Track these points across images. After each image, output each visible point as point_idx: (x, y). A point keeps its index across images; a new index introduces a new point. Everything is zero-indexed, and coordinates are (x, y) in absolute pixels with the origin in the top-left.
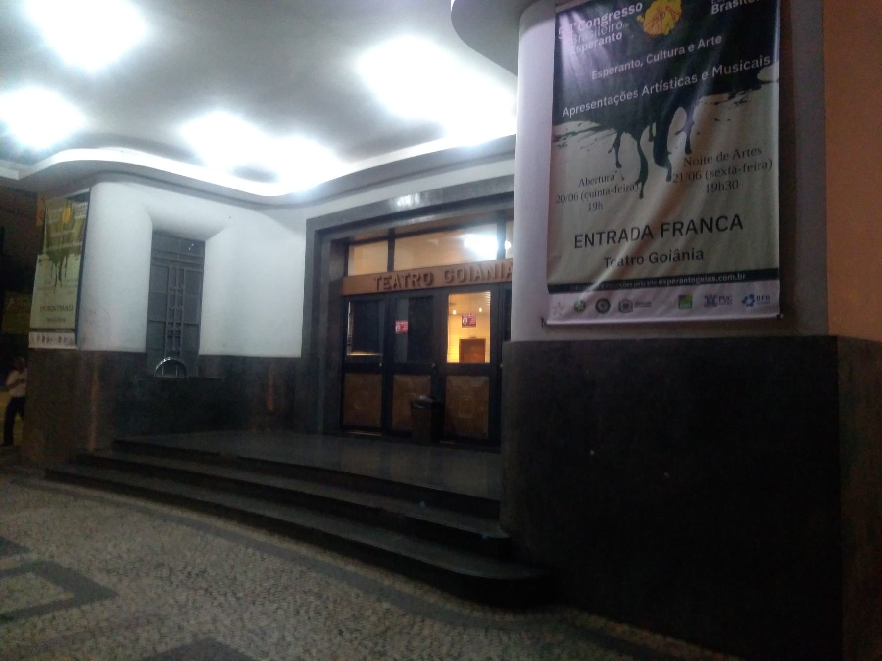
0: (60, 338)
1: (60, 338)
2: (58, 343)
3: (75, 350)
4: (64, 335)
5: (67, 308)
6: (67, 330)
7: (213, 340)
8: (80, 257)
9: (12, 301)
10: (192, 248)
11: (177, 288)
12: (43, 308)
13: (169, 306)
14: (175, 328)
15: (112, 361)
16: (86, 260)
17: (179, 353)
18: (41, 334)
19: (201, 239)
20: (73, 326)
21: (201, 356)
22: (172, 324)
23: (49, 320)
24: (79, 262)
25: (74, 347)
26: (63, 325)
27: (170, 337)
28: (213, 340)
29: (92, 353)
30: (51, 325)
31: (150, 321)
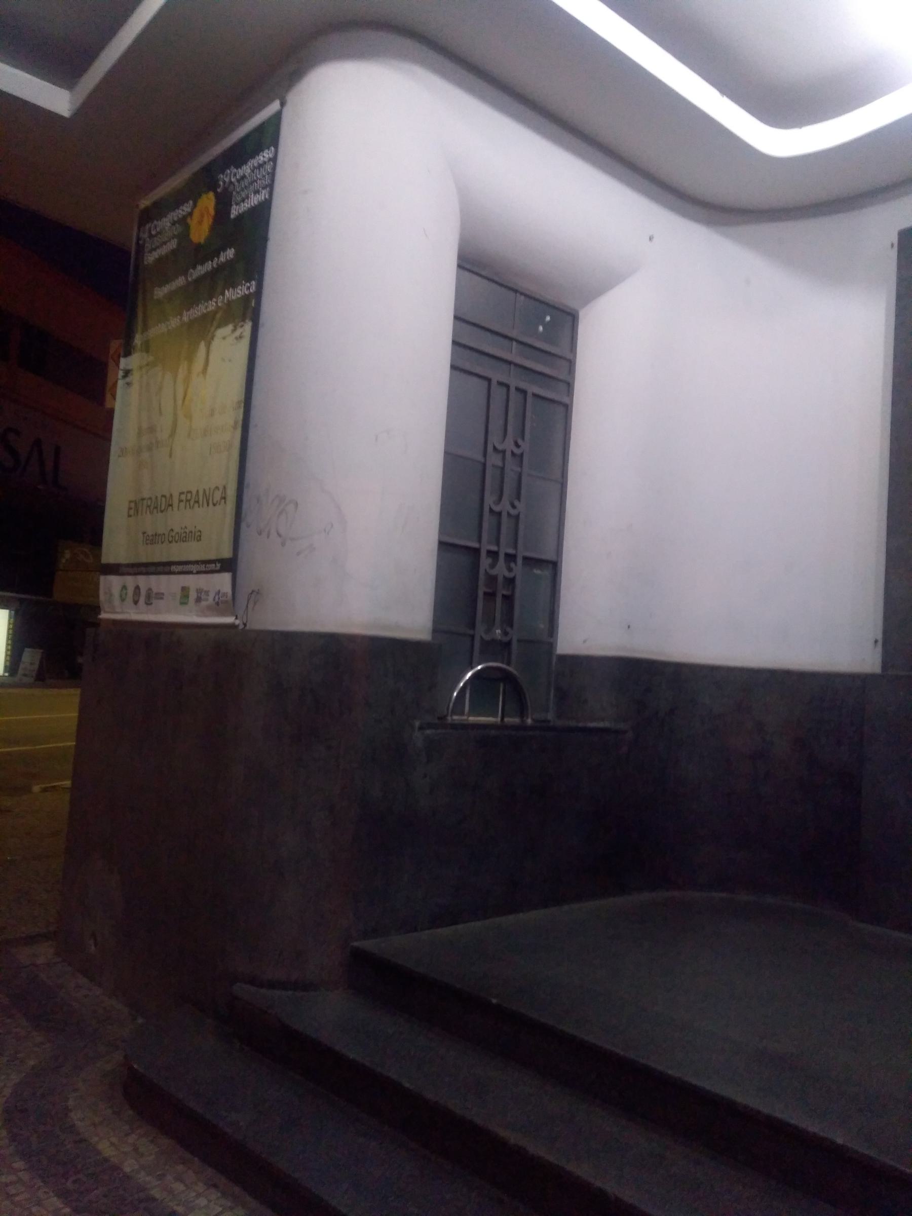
0: (185, 590)
1: (185, 590)
2: (179, 605)
3: (232, 626)
4: (193, 582)
5: (206, 499)
6: (209, 566)
7: (595, 616)
8: (248, 327)
9: (68, 555)
10: (541, 321)
11: (509, 445)
12: (136, 507)
13: (489, 500)
14: (501, 569)
15: (343, 659)
16: (262, 332)
17: (508, 644)
18: (130, 581)
19: (570, 302)
20: (227, 553)
21: (563, 658)
22: (493, 555)
23: (153, 539)
24: (243, 347)
25: (229, 620)
26: (193, 551)
27: (490, 596)
28: (595, 616)
29: (288, 642)
30: (159, 554)
31: (444, 546)
